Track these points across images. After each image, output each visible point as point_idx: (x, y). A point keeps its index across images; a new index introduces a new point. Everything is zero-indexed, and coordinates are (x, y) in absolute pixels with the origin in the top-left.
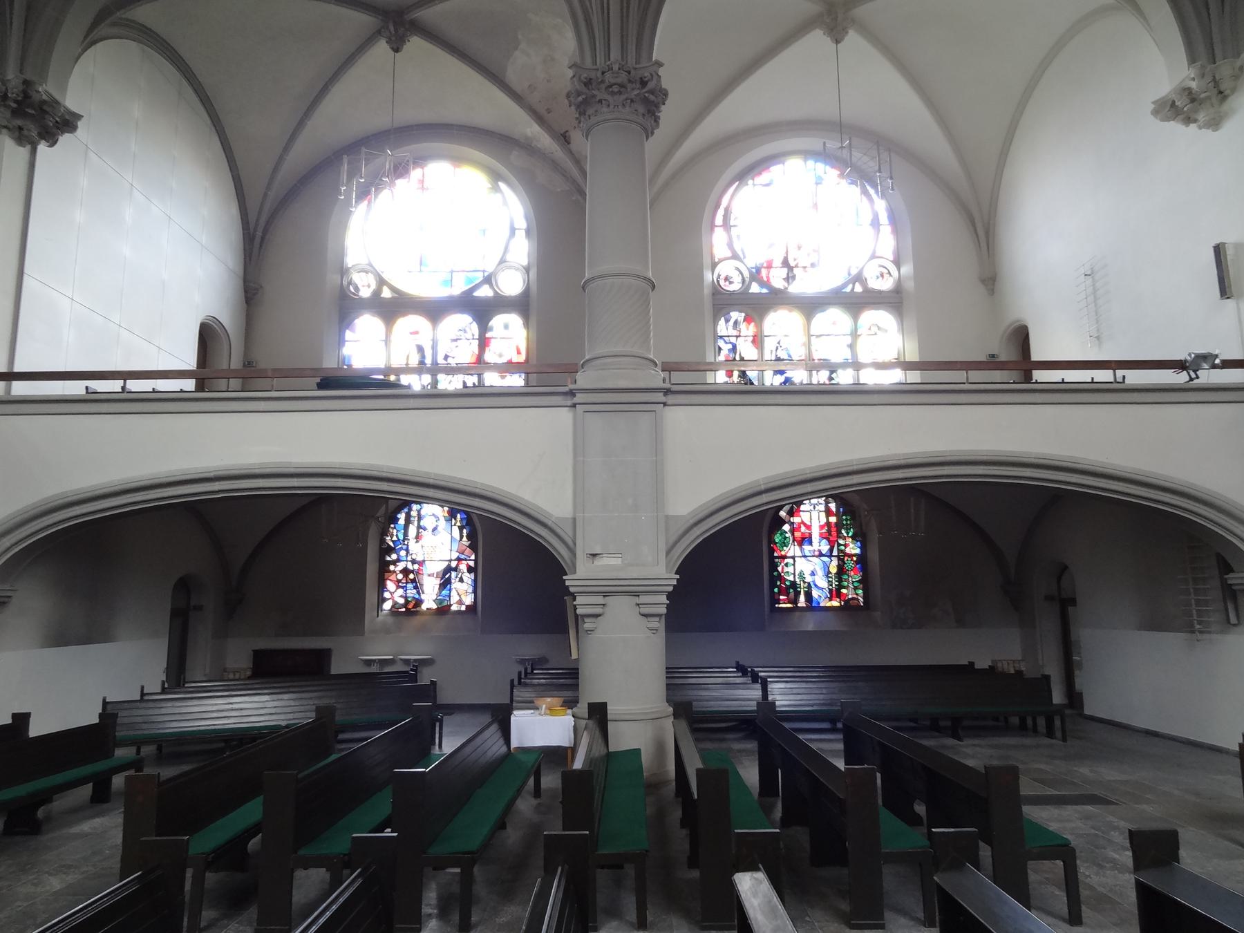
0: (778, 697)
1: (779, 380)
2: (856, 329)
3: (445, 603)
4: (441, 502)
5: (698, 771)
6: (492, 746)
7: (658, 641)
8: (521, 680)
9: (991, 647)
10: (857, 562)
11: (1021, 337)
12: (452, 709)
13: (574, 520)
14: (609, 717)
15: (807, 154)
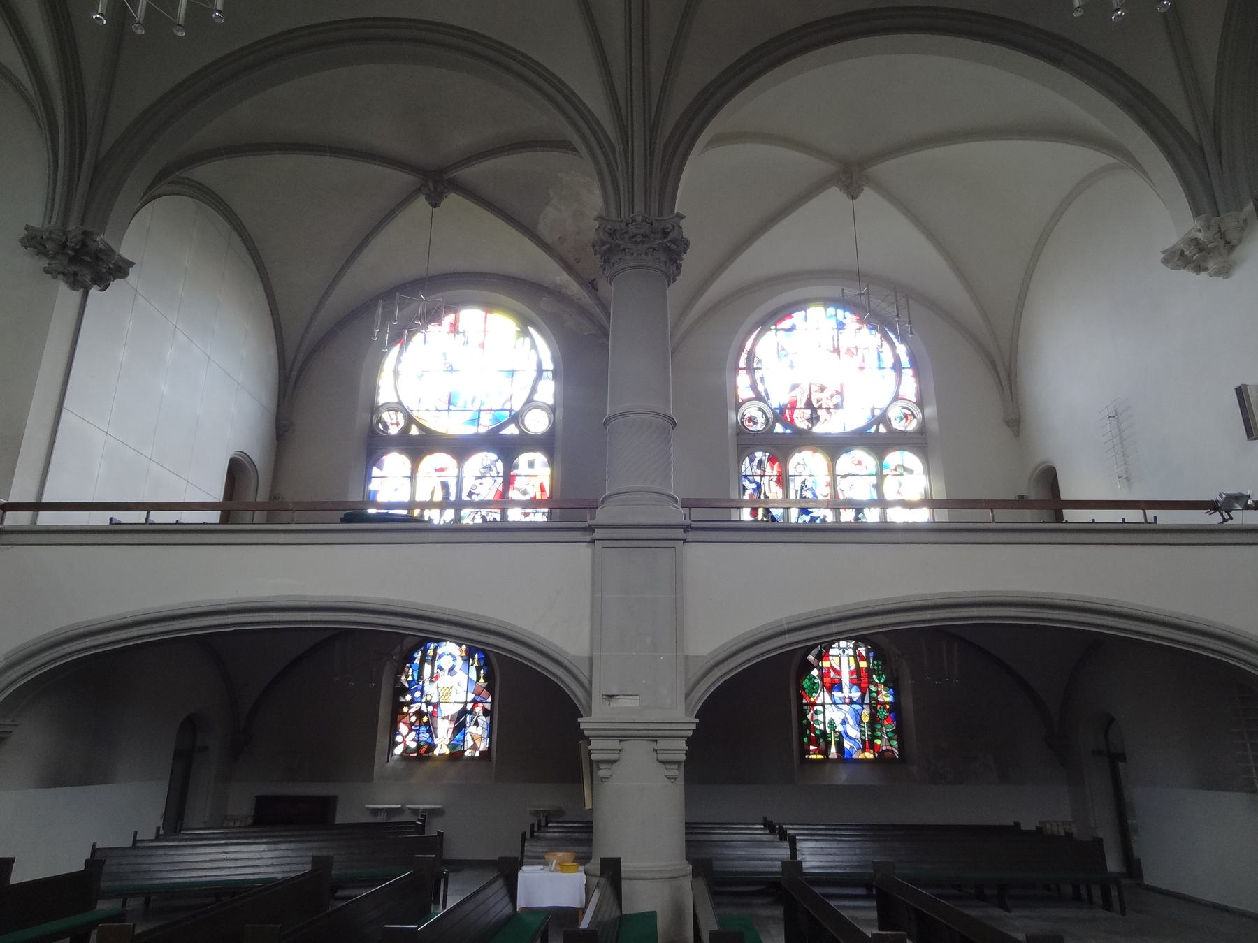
0: (808, 858)
1: (807, 519)
2: (882, 471)
3: (459, 748)
4: (459, 641)
5: (712, 934)
6: (500, 908)
7: (676, 792)
8: (534, 833)
9: (1038, 806)
10: (890, 711)
11: (1049, 477)
12: (460, 866)
13: (591, 659)
14: (623, 875)
15: (827, 301)
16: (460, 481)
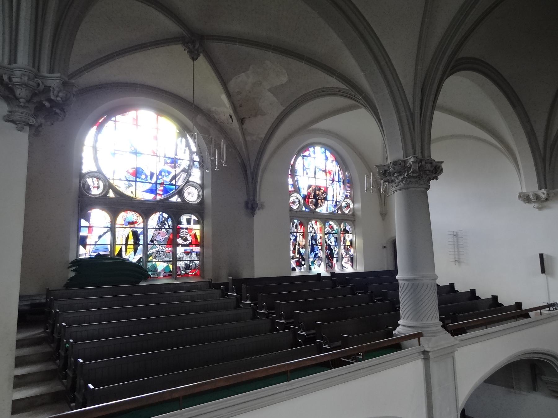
16: (146, 229)
